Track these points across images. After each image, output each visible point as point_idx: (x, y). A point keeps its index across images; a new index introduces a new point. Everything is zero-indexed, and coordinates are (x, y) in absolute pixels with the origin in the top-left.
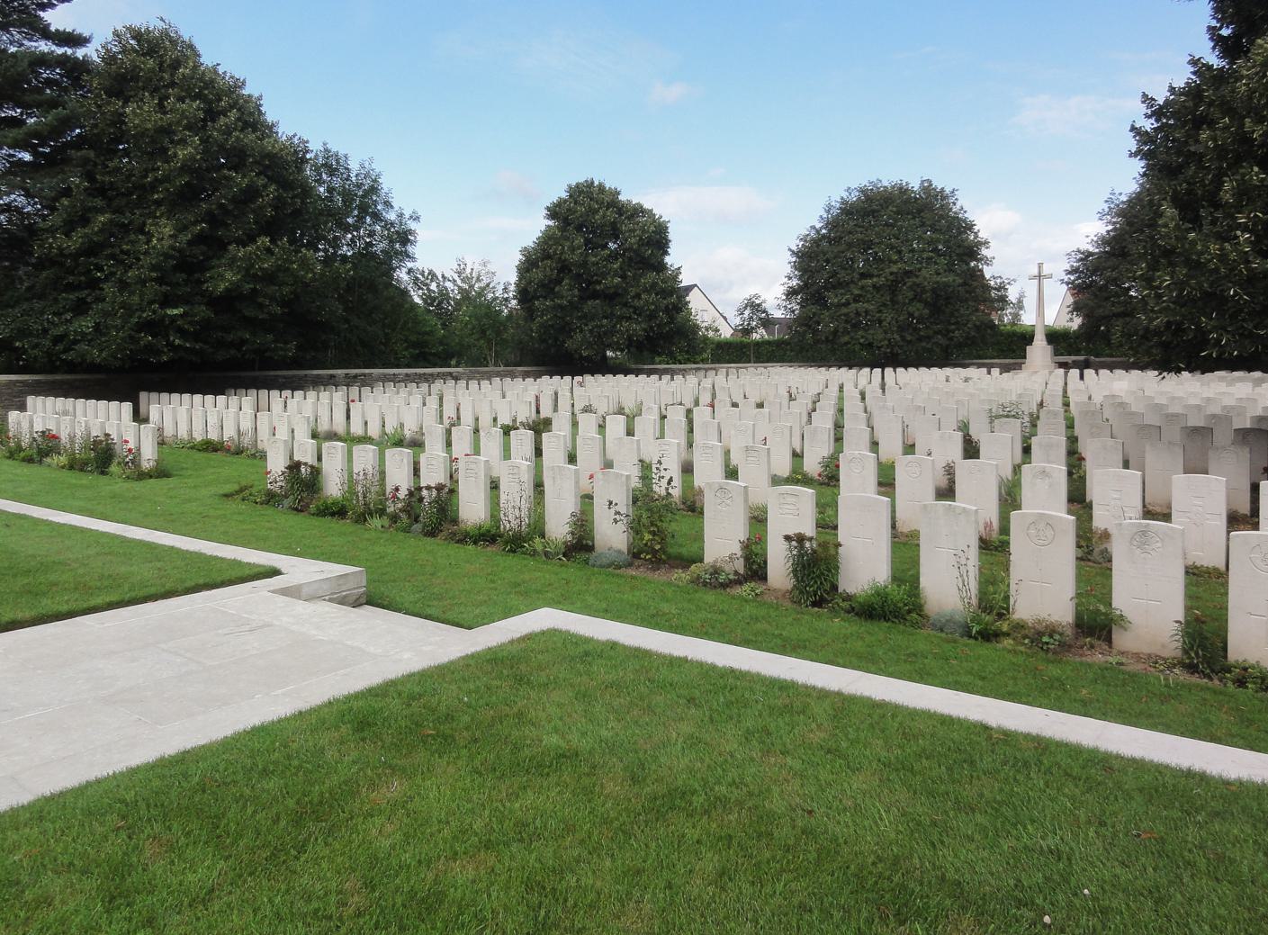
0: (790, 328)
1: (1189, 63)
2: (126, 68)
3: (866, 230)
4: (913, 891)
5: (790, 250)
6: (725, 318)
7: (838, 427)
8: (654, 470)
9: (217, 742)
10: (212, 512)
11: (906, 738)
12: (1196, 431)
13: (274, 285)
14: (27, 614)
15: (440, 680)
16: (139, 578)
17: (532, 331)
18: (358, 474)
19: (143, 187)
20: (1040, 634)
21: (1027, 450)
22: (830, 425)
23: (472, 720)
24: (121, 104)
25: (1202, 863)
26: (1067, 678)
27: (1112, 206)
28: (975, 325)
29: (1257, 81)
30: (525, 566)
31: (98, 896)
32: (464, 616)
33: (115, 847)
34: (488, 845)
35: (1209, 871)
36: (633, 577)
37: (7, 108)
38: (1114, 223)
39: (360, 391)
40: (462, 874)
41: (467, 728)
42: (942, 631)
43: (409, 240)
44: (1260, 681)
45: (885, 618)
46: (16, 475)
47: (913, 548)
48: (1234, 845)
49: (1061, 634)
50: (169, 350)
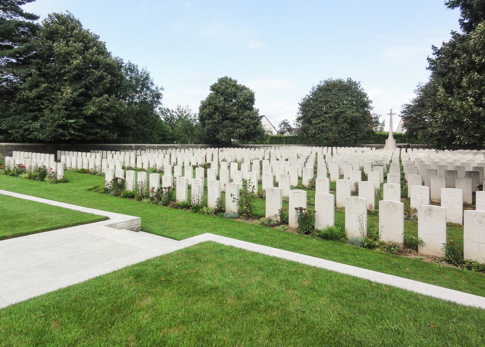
0: (298, 132)
1: (451, 33)
2: (53, 29)
3: (327, 96)
4: (343, 344)
5: (299, 103)
6: (275, 128)
7: (315, 168)
8: (248, 183)
9: (82, 283)
10: (84, 196)
11: (340, 285)
12: (450, 172)
13: (110, 112)
14: (10, 234)
15: (168, 259)
16: (55, 220)
17: (204, 131)
18: (139, 183)
19: (60, 74)
20: (390, 247)
21: (385, 178)
22: (312, 167)
23: (179, 274)
24: (51, 43)
25: (456, 339)
26: (401, 264)
27: (419, 88)
28: (366, 132)
29: (478, 40)
30: (200, 217)
31: (31, 344)
32: (177, 235)
33: (39, 324)
34: (183, 323)
35: (459, 342)
36: (239, 222)
37: (6, 42)
38: (420, 94)
39: (141, 152)
40: (173, 333)
41: (177, 278)
42: (353, 244)
43: (160, 97)
44: (477, 268)
45: (332, 239)
46: (8, 181)
47: (343, 213)
48: (468, 332)
49: (398, 247)
50: (69, 135)
